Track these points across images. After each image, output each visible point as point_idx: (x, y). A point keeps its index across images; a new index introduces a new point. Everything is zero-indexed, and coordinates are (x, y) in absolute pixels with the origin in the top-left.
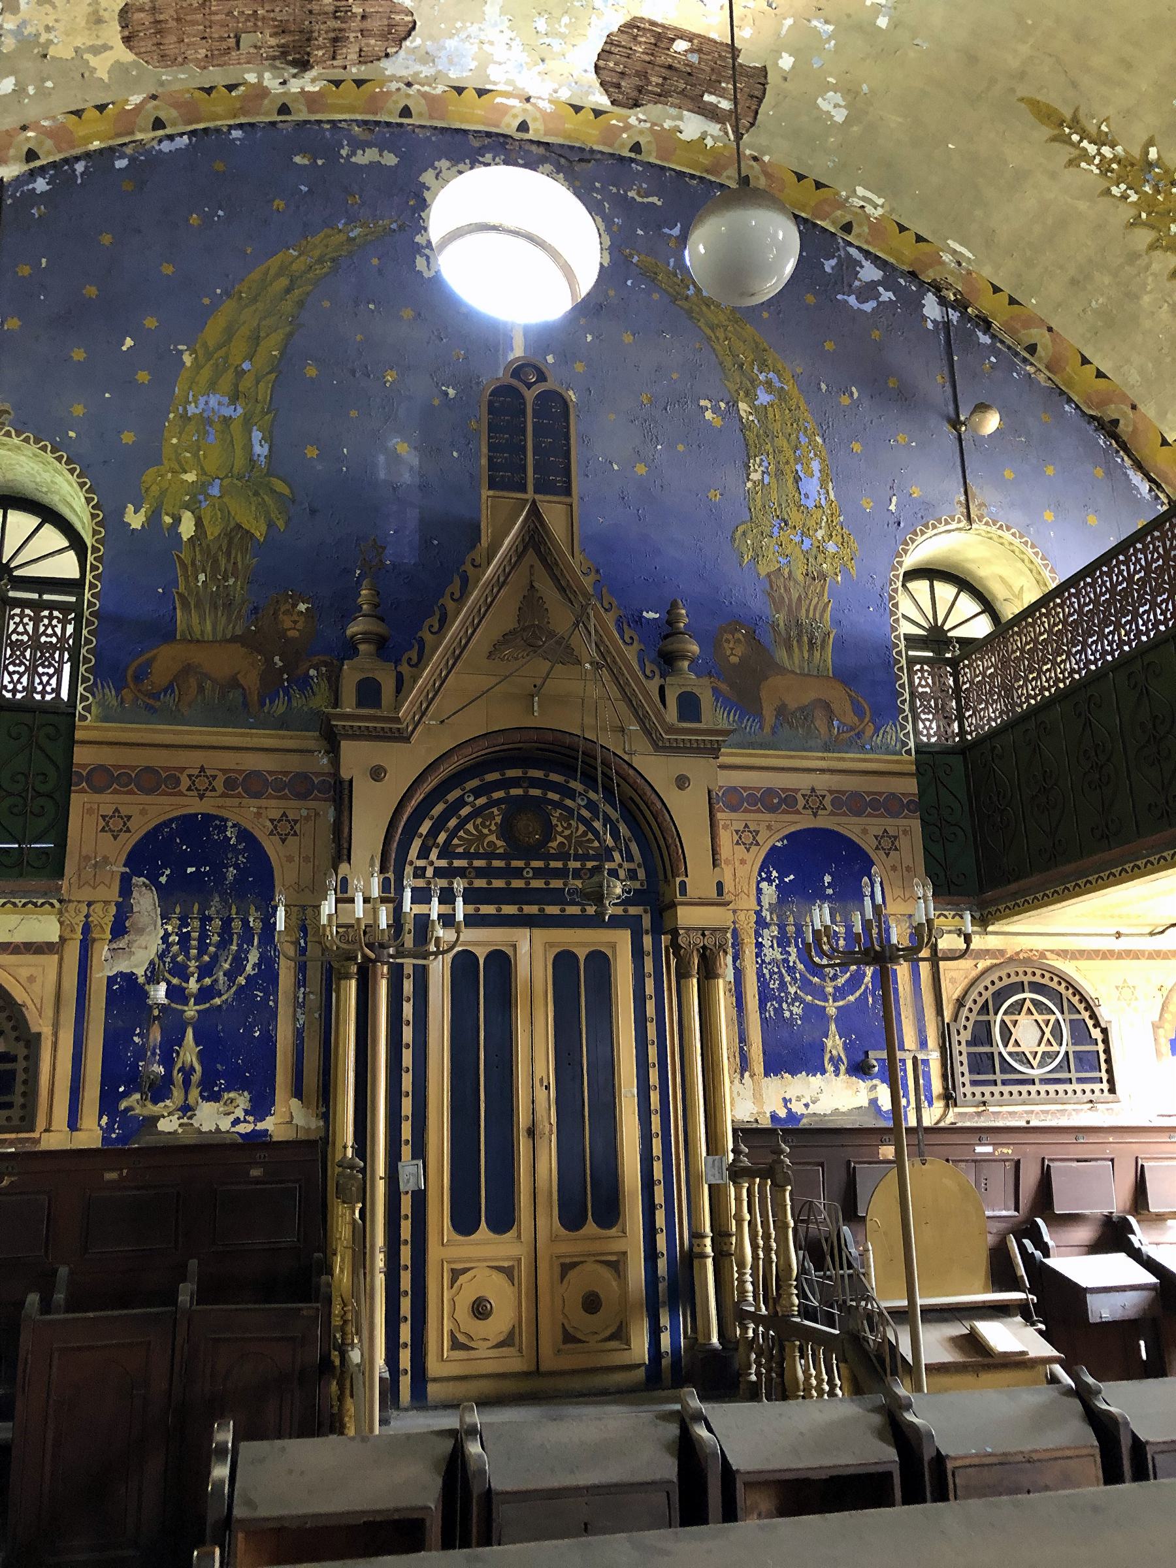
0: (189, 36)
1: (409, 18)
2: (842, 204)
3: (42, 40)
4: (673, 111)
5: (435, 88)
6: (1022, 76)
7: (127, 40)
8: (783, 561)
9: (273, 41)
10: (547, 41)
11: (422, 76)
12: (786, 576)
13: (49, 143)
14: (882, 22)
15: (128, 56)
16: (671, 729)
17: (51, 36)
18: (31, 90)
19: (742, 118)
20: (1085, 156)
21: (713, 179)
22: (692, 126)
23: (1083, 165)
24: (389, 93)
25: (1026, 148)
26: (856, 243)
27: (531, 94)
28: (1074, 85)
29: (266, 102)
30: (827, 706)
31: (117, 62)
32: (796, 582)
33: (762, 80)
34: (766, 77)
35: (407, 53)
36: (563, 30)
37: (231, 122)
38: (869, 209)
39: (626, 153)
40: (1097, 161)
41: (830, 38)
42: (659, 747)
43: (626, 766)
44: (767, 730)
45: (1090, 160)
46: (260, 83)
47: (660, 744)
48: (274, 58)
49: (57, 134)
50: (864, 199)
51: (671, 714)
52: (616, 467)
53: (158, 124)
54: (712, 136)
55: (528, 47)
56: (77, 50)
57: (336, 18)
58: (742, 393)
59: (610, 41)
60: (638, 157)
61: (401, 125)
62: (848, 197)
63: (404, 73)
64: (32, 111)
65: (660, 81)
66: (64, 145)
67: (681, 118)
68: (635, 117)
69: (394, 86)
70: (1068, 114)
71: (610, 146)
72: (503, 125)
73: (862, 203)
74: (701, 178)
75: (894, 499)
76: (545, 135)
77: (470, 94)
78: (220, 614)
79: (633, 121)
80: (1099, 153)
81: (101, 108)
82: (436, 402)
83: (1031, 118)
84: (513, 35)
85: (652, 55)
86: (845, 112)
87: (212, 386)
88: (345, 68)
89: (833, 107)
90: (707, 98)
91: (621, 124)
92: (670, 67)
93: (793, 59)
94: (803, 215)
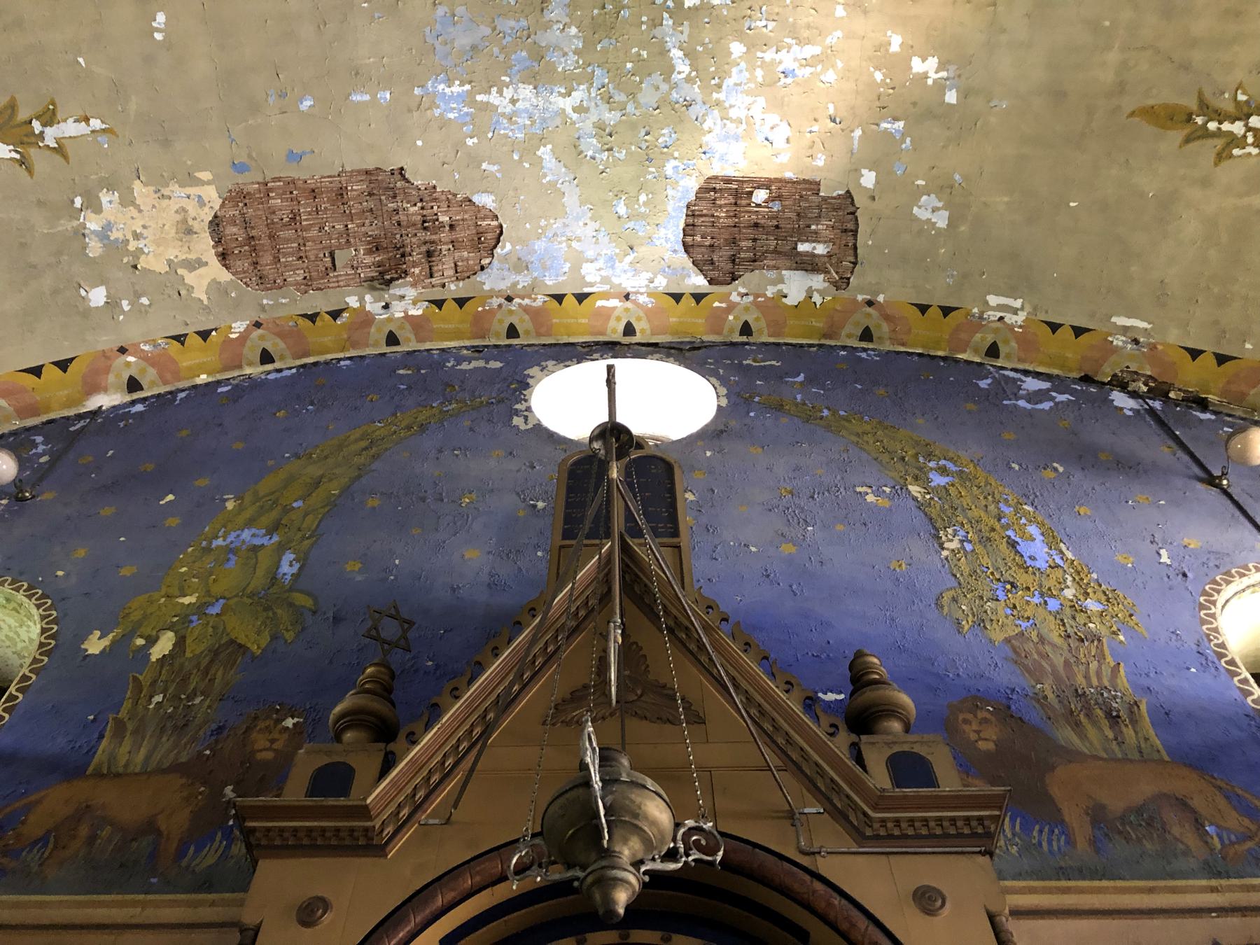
0: (285, 255)
1: (495, 223)
2: (978, 323)
3: (132, 247)
4: (772, 274)
5: (535, 300)
6: (1121, 88)
7: (223, 257)
8: (1025, 624)
9: (368, 260)
10: (631, 225)
11: (520, 287)
12: (1035, 639)
13: (152, 373)
14: (951, 97)
15: (225, 276)
16: (880, 801)
17: (141, 244)
18: (125, 305)
19: (842, 265)
20: (1234, 141)
21: (832, 343)
22: (796, 287)
23: (1236, 152)
24: (491, 312)
25: (1160, 165)
26: (1009, 366)
27: (630, 290)
28: (1185, 67)
29: (373, 330)
30: (1182, 804)
31: (214, 280)
32: (1054, 646)
33: (851, 209)
34: (853, 203)
35: (499, 261)
36: (643, 209)
37: (341, 355)
38: (1010, 319)
39: (737, 338)
40: (1250, 140)
41: (904, 135)
42: (870, 835)
43: (807, 878)
44: (1082, 845)
45: (1240, 142)
46: (363, 306)
47: (869, 832)
48: (372, 279)
49: (158, 361)
50: (1000, 307)
51: (879, 777)
52: (753, 549)
53: (266, 357)
54: (818, 291)
55: (615, 236)
56: (170, 262)
57: (425, 229)
58: (909, 479)
59: (691, 214)
60: (751, 340)
61: (510, 346)
62: (982, 313)
63: (503, 286)
64: (131, 333)
65: (750, 244)
66: (168, 376)
67: (781, 280)
68: (736, 293)
69: (495, 302)
70: (1193, 105)
71: (719, 333)
72: (609, 331)
73: (999, 314)
74: (821, 346)
75: (1163, 552)
76: (653, 334)
77: (570, 301)
78: (164, 739)
79: (735, 298)
80: (1249, 129)
81: (204, 335)
82: (521, 514)
83: (1149, 129)
84: (597, 225)
85: (735, 216)
86: (946, 214)
87: (250, 523)
88: (443, 286)
89: (931, 212)
90: (803, 247)
91: (724, 305)
92: (756, 225)
93: (873, 174)
94: (940, 353)
